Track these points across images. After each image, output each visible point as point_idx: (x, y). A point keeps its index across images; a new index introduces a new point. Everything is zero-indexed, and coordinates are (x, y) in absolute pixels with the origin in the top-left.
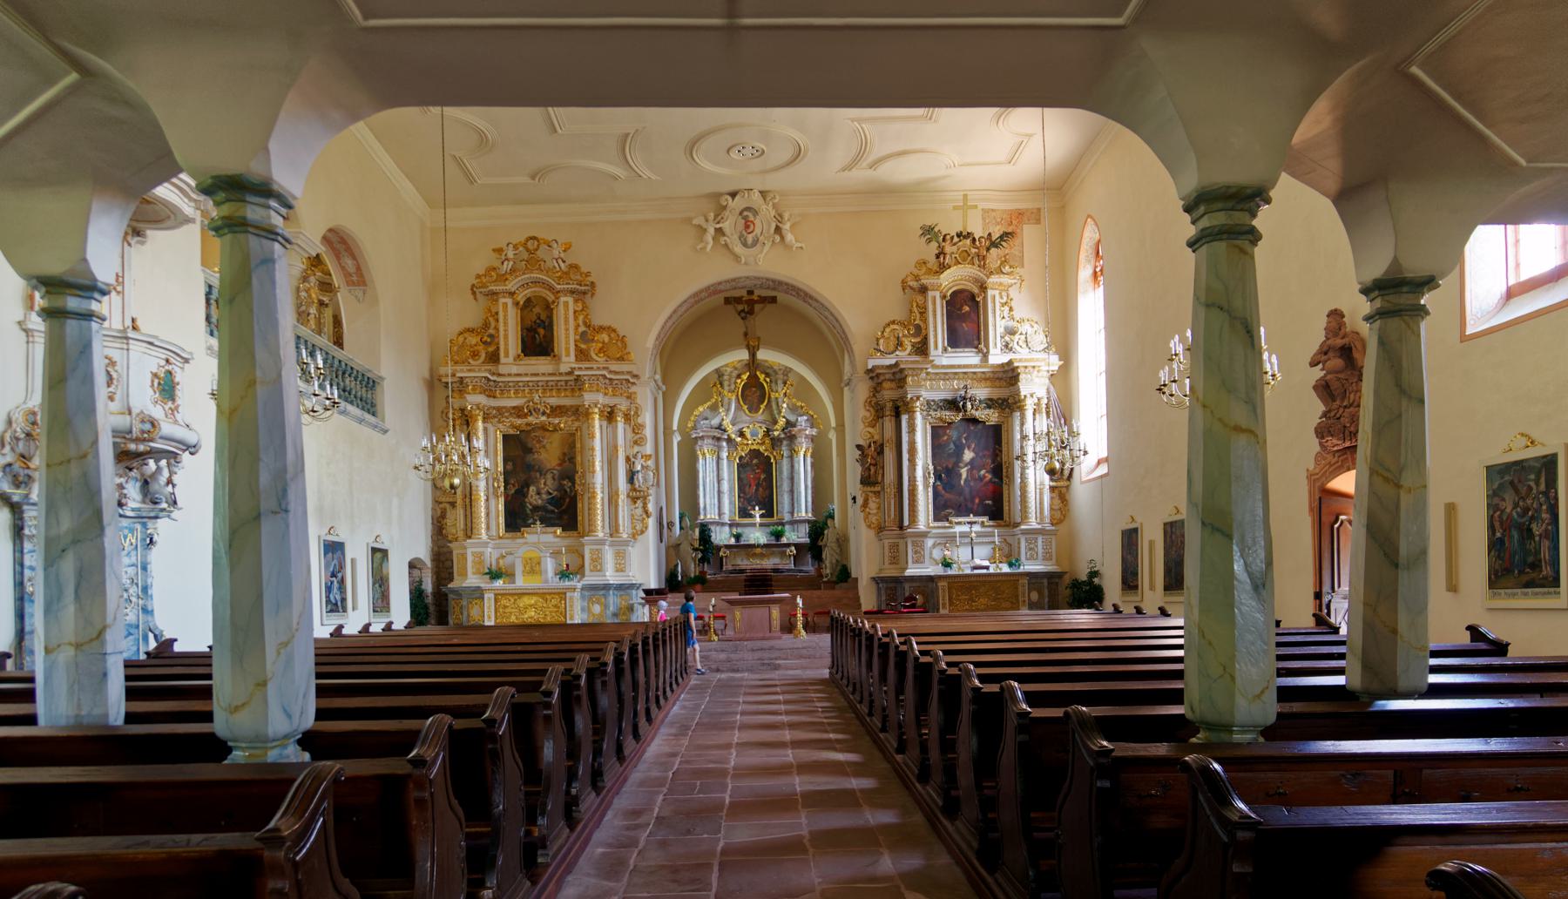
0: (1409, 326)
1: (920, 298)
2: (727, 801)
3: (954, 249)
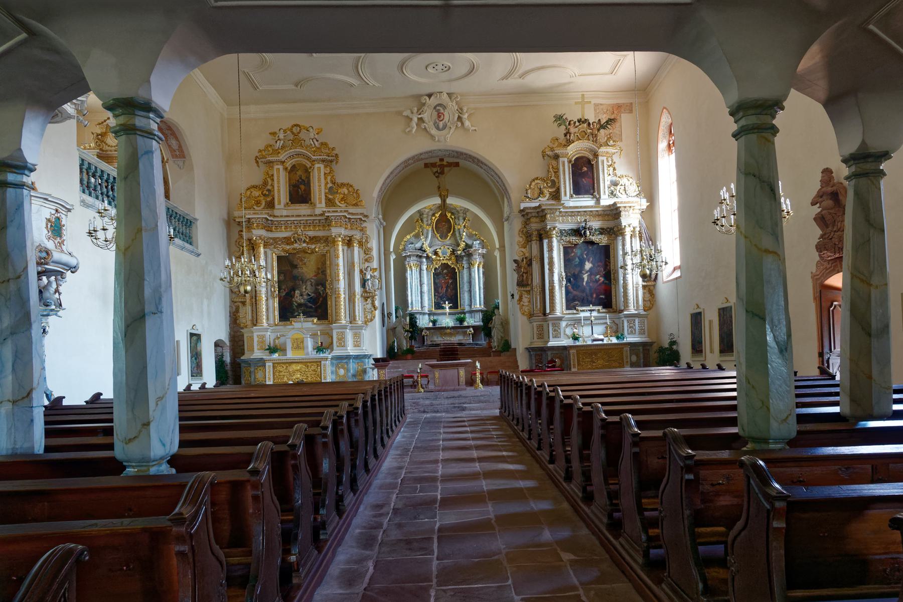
0: (873, 183)
1: (554, 162)
2: (439, 497)
3: (577, 130)
